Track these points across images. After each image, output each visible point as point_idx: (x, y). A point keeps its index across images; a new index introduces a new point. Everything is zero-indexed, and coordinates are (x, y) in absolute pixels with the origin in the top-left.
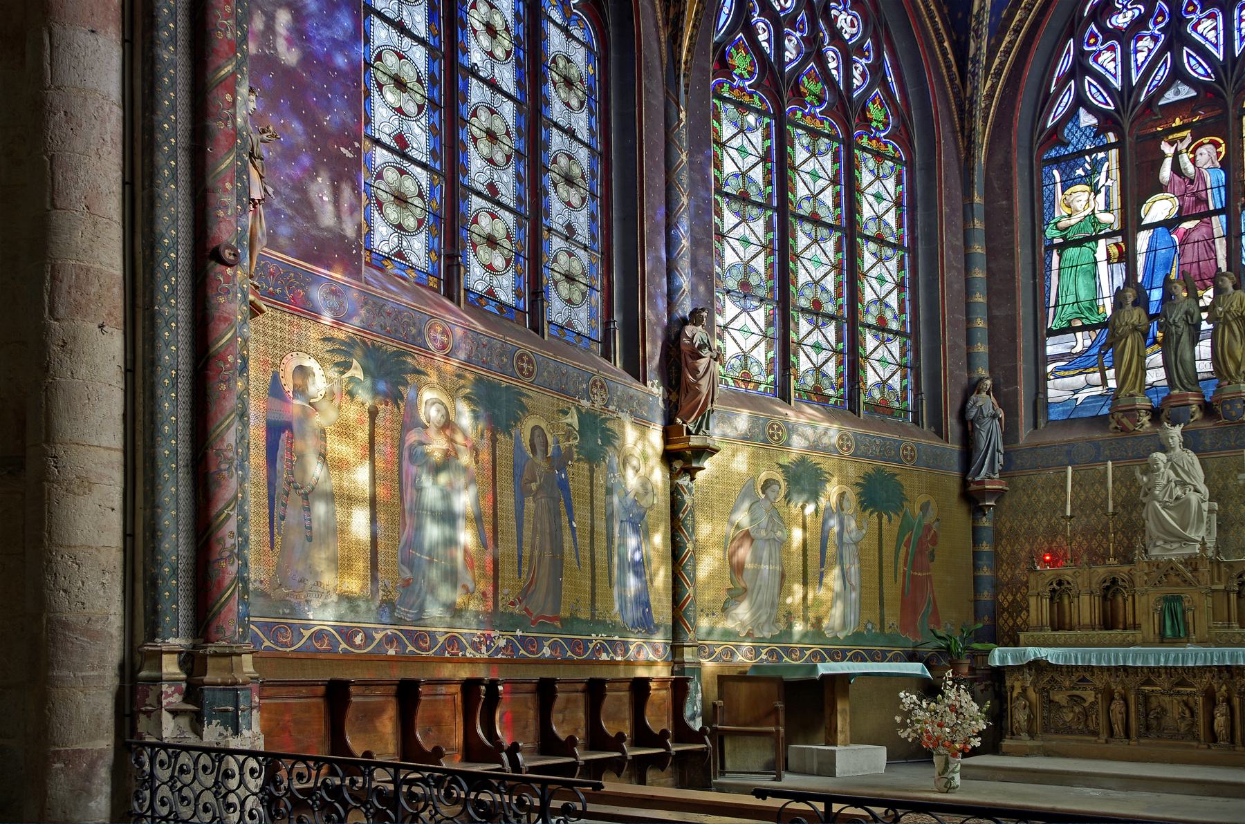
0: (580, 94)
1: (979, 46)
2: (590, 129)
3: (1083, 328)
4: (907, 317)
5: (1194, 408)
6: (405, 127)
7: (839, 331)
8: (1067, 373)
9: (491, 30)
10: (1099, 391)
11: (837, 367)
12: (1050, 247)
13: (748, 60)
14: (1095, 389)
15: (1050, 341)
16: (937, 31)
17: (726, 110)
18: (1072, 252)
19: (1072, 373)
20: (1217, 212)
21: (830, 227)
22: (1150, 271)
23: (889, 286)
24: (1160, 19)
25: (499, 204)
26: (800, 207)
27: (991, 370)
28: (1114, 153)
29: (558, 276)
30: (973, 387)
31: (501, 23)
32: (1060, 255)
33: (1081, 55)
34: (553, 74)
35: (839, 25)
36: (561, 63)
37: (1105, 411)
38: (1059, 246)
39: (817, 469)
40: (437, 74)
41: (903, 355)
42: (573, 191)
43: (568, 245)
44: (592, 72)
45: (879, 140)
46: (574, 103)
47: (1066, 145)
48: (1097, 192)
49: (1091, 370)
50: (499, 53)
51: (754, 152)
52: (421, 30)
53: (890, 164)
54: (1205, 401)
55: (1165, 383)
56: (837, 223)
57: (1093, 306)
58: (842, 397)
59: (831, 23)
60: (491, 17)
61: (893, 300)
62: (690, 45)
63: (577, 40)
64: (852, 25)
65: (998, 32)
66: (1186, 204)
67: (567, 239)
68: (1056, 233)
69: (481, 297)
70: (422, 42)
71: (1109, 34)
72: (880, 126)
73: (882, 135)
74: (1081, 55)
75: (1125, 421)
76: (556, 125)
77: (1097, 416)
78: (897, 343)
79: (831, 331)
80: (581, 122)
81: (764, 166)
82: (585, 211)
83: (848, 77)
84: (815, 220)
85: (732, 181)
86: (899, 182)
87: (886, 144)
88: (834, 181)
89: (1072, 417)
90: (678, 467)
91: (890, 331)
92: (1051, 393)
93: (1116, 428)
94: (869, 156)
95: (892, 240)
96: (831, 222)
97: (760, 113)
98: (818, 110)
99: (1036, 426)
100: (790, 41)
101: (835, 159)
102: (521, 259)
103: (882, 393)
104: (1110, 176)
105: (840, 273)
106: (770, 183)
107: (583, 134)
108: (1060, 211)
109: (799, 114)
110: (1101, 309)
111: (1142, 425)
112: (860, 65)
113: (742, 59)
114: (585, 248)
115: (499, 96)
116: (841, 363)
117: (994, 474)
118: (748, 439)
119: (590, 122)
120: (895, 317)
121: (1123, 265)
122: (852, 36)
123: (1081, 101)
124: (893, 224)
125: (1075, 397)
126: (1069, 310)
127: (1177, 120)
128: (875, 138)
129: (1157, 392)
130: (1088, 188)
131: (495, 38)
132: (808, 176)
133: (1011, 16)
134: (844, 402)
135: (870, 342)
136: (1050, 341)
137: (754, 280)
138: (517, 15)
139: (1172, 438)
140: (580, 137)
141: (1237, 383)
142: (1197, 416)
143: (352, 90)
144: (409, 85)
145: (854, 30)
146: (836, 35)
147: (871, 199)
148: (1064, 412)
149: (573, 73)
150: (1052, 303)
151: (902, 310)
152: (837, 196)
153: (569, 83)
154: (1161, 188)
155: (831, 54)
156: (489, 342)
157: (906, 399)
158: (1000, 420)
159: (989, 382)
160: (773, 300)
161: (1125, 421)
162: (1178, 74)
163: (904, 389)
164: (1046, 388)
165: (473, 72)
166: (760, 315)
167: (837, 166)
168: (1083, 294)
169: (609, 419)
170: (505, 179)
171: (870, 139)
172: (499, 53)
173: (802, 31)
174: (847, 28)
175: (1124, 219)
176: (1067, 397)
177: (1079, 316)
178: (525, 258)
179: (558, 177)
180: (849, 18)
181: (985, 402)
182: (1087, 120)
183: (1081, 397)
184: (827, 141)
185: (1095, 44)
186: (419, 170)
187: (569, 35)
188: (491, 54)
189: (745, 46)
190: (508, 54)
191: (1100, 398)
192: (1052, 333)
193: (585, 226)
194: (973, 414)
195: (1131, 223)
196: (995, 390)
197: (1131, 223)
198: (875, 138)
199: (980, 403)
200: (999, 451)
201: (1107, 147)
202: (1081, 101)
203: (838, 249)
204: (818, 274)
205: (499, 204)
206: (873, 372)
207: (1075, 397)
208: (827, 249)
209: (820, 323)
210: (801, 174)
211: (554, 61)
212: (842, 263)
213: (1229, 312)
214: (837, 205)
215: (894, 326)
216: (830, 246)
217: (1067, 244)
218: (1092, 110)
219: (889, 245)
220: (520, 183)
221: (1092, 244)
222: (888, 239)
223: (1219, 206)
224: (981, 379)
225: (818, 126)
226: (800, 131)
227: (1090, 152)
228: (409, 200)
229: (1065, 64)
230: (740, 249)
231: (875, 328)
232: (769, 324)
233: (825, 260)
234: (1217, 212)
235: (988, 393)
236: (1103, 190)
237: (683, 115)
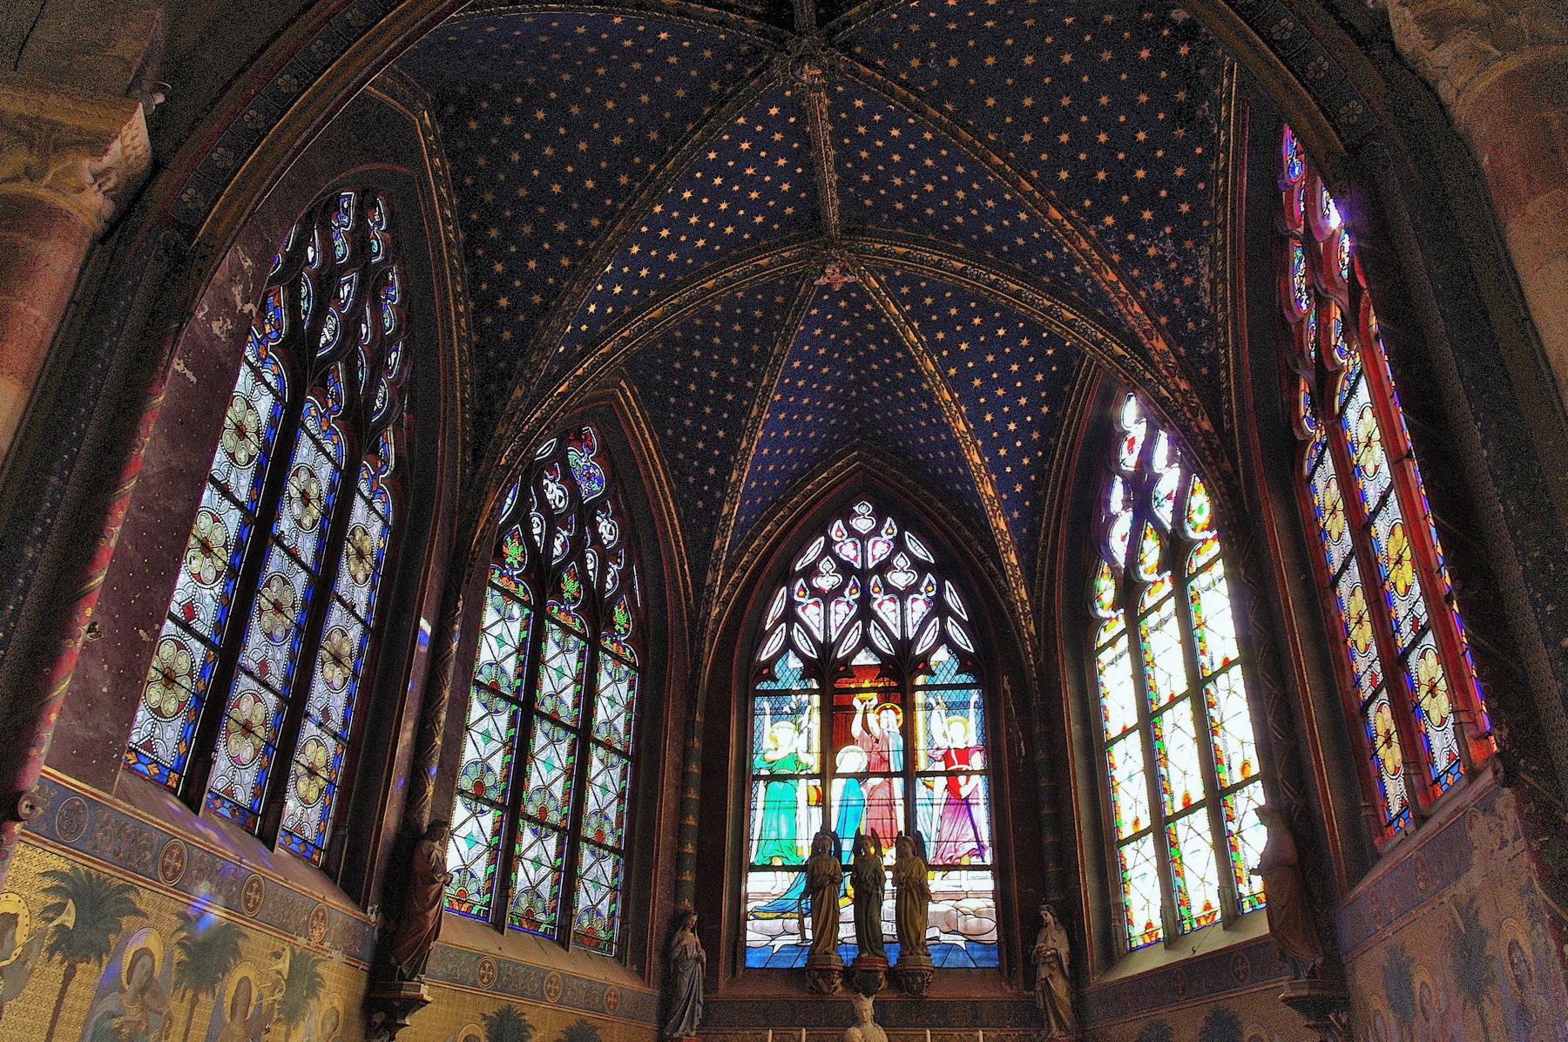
0: (367, 567)
1: (715, 578)
2: (369, 604)
3: (784, 868)
4: (622, 832)
5: (881, 975)
6: (197, 596)
7: (560, 843)
8: (766, 915)
9: (305, 498)
10: (795, 939)
11: (552, 887)
12: (759, 777)
13: (520, 550)
14: (791, 937)
15: (752, 876)
16: (680, 553)
17: (492, 596)
18: (775, 785)
19: (770, 915)
20: (897, 775)
21: (567, 728)
22: (844, 822)
23: (611, 796)
24: (854, 591)
25: (266, 685)
26: (543, 704)
27: (696, 902)
28: (816, 699)
29: (301, 769)
30: (677, 922)
31: (315, 491)
32: (766, 787)
33: (791, 605)
34: (349, 545)
35: (600, 531)
36: (358, 535)
37: (800, 963)
38: (765, 778)
39: (521, 1021)
40: (245, 540)
41: (615, 875)
42: (338, 670)
43: (319, 731)
44: (382, 545)
45: (619, 643)
46: (361, 576)
47: (776, 680)
48: (800, 732)
49: (788, 915)
50: (307, 521)
51: (511, 642)
52: (243, 494)
53: (626, 668)
54: (889, 968)
55: (854, 940)
56: (573, 725)
57: (794, 849)
58: (552, 924)
59: (595, 525)
60: (309, 485)
61: (612, 813)
62: (480, 537)
63: (377, 512)
64: (611, 534)
65: (730, 567)
66: (873, 761)
67: (320, 725)
68: (764, 764)
69: (218, 797)
70: (239, 505)
71: (815, 592)
72: (622, 629)
73: (623, 639)
74: (791, 605)
75: (820, 981)
76: (340, 599)
77: (791, 969)
78: (611, 861)
79: (552, 844)
80: (361, 597)
81: (517, 658)
82: (344, 694)
83: (602, 580)
84: (554, 719)
85: (486, 670)
86: (631, 688)
87: (624, 648)
88: (577, 681)
89: (768, 966)
90: (378, 1021)
91: (605, 847)
92: (750, 936)
93: (811, 988)
94: (609, 658)
95: (619, 747)
96: (569, 723)
97: (524, 604)
98: (572, 608)
99: (734, 974)
100: (558, 538)
101: (581, 658)
102: (271, 750)
103: (590, 920)
104: (813, 721)
105: (569, 779)
106: (520, 676)
107: (361, 610)
108: (767, 743)
109: (556, 608)
110: (799, 851)
111: (836, 988)
112: (614, 569)
113: (515, 548)
114: (335, 736)
115: (296, 566)
116: (557, 882)
117: (692, 1030)
118: (457, 981)
119: (370, 598)
120: (612, 832)
121: (820, 809)
122: (610, 542)
123: (789, 644)
124: (621, 730)
125: (772, 943)
126: (771, 846)
127: (867, 681)
128: (616, 641)
129: (846, 950)
130: (793, 726)
131: (307, 506)
132: (554, 672)
133: (740, 557)
134: (553, 930)
135: (587, 859)
136: (752, 876)
137: (489, 781)
138: (332, 484)
139: (866, 1010)
140: (358, 612)
141: (918, 954)
142: (884, 984)
143: (172, 565)
144: (215, 550)
145: (611, 538)
146: (597, 538)
147: (605, 701)
148: (761, 959)
149: (367, 546)
150: (756, 837)
151: (619, 824)
152: (577, 695)
153: (360, 555)
154: (851, 741)
155: (589, 556)
156: (223, 867)
157: (612, 927)
158: (702, 964)
159: (695, 918)
160: (503, 804)
161: (820, 981)
162: (866, 642)
163: (612, 915)
164: (745, 929)
165: (279, 540)
166: (488, 821)
167: (580, 664)
168: (784, 833)
169: (319, 961)
170: (278, 657)
171: (612, 642)
172: (307, 521)
173: (570, 531)
174: (606, 534)
175: (823, 765)
176: (765, 943)
177: (779, 854)
178: (274, 749)
179: (328, 655)
180: (609, 526)
181: (691, 939)
182: (794, 663)
183: (778, 944)
184: (575, 638)
185: (803, 597)
186: (198, 644)
187: (372, 508)
188: (299, 522)
189: (520, 538)
190: (251, 458)
191: (795, 948)
192: (753, 868)
193: (341, 711)
194: (677, 954)
195: (827, 772)
196: (699, 929)
197: (827, 772)
198: (616, 641)
199: (685, 942)
200: (699, 1002)
201: (811, 692)
202: (789, 644)
203: (571, 753)
204: (547, 779)
205: (266, 685)
206: (549, 853)
207: (772, 943)
208: (560, 752)
209: (543, 834)
210: (549, 669)
211: (353, 533)
212: (573, 769)
213: (910, 877)
214: (576, 705)
215: (610, 841)
216: (563, 748)
217: (773, 777)
218: (799, 654)
219: (616, 751)
220: (291, 662)
221: (794, 782)
222: (615, 746)
223: (899, 770)
224: (687, 914)
225: (569, 622)
226: (554, 626)
227: (796, 693)
228: (178, 680)
229: (777, 608)
230: (481, 744)
231: (593, 843)
232: (496, 833)
233: (557, 764)
234: (897, 775)
235: (693, 931)
236: (806, 731)
237: (460, 604)
